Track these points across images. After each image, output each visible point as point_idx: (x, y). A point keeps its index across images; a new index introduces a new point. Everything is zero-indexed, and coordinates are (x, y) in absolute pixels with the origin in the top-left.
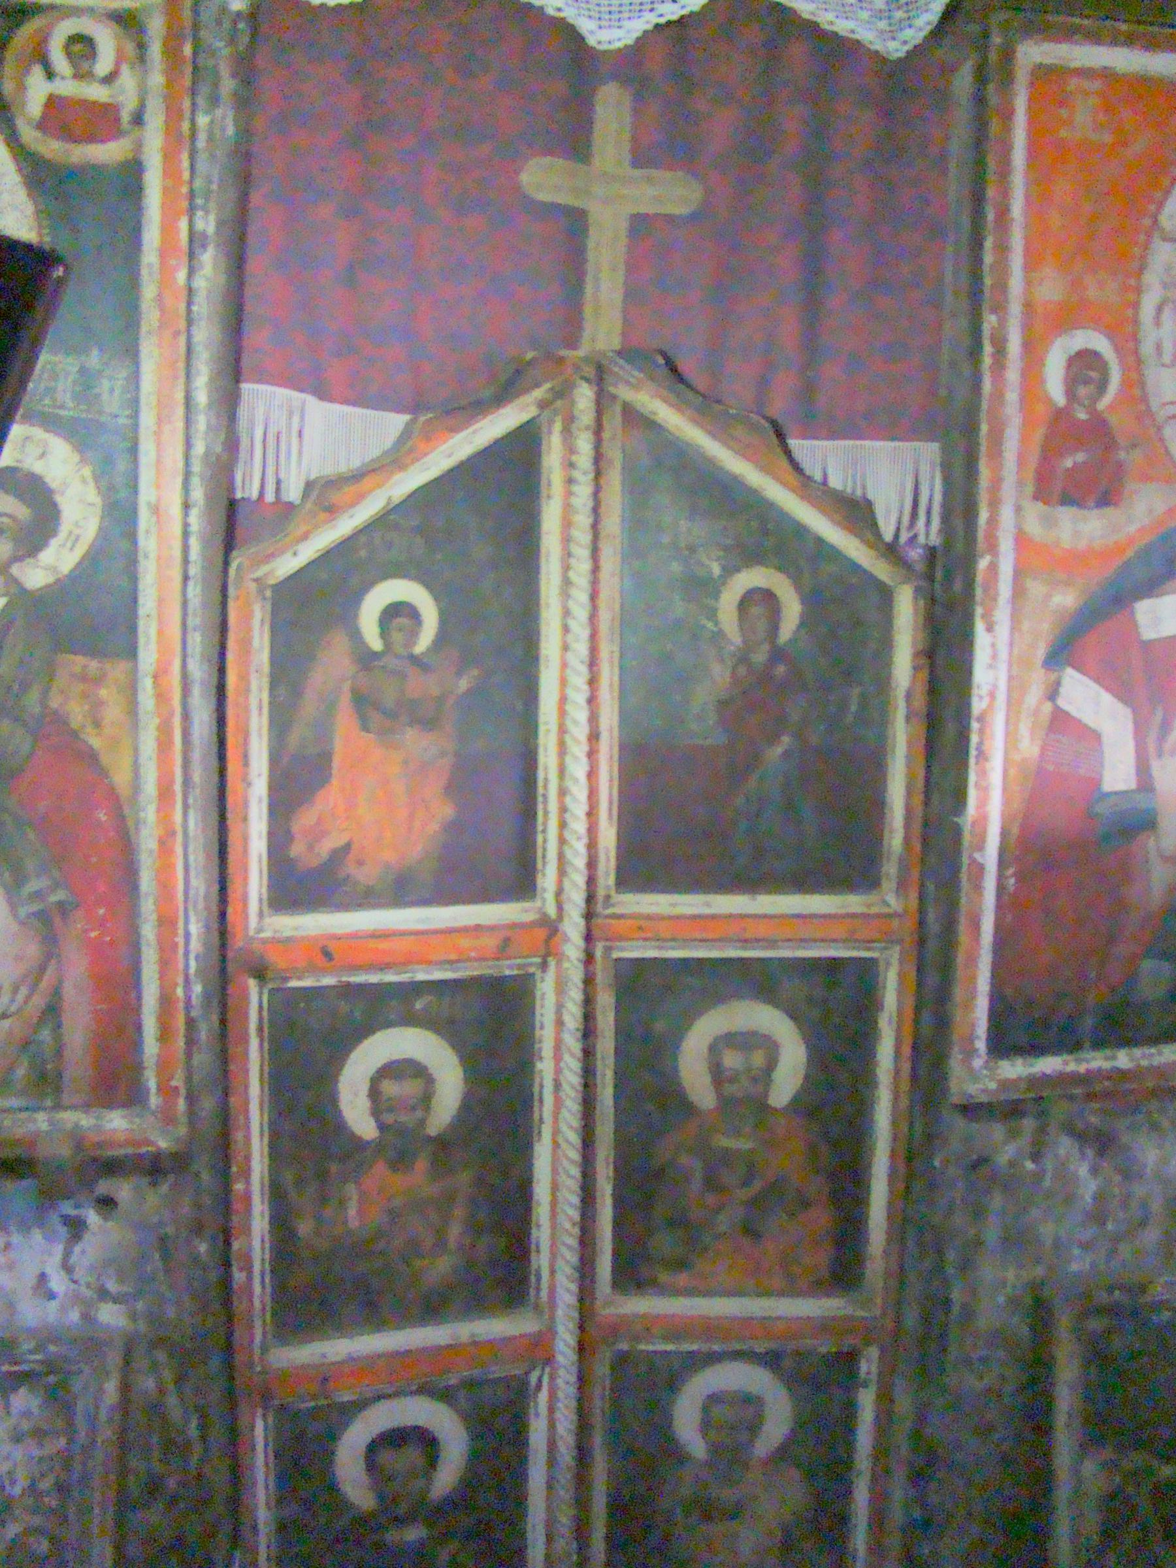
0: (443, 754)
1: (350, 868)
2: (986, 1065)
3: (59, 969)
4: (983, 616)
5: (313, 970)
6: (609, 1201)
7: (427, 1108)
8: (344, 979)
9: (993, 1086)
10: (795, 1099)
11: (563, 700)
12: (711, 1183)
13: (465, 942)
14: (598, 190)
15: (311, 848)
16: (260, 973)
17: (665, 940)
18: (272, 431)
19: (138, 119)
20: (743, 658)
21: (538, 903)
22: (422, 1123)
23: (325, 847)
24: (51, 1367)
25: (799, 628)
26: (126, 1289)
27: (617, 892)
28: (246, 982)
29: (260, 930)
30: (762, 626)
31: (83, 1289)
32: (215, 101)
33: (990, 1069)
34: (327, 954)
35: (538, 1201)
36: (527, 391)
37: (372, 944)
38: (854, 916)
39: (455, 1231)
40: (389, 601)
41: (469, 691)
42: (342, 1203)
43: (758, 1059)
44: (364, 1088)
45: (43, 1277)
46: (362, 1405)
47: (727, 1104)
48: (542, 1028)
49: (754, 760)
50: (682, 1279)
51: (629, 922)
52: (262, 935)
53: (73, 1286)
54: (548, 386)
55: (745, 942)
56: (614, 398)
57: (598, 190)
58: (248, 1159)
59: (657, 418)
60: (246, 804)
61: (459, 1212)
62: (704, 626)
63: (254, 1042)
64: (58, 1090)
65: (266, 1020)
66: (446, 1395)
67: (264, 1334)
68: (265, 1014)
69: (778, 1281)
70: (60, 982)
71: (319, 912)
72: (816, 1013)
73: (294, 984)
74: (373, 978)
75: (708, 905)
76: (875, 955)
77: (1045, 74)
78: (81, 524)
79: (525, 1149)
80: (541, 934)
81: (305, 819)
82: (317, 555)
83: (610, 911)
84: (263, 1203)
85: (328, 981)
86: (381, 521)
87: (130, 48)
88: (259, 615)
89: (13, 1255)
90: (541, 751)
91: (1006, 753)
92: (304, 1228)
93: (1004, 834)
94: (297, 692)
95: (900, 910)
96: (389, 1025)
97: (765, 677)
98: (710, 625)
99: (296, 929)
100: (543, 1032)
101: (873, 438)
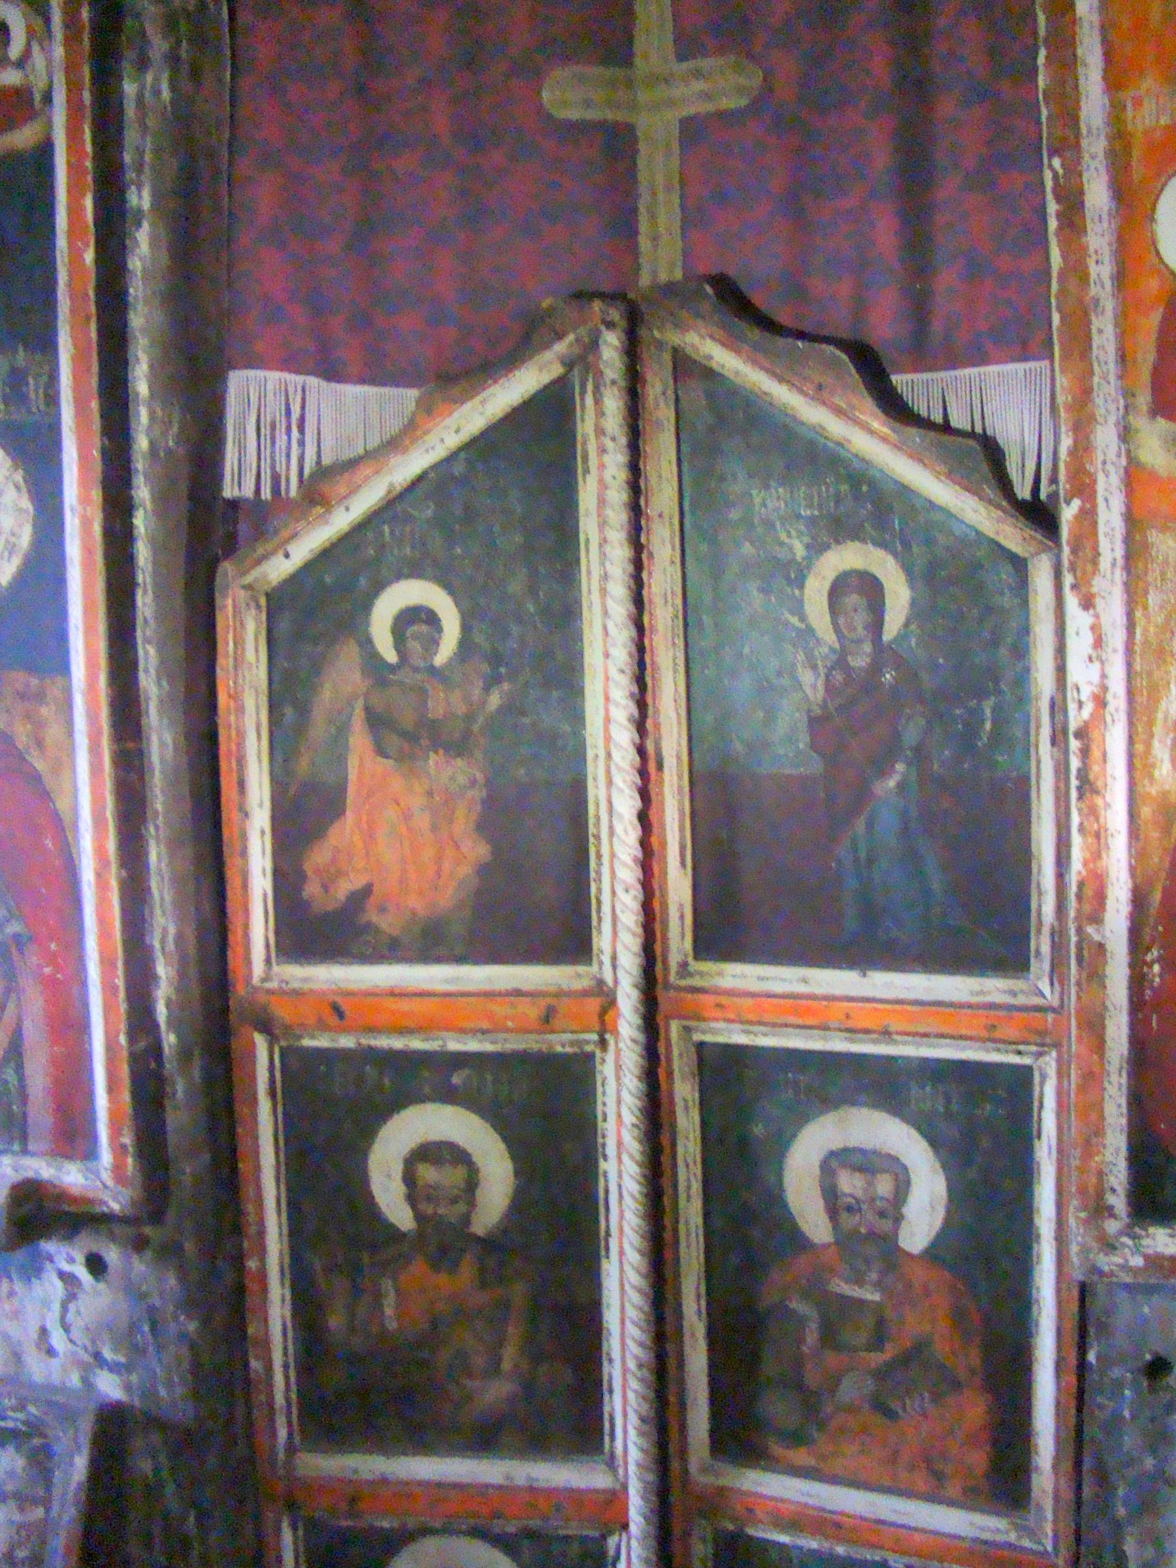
0: (473, 782)
2: (1128, 1231)
3: (19, 1006)
4: (1074, 587)
6: (702, 1345)
7: (472, 1204)
8: (364, 1041)
9: (1137, 1261)
11: (607, 720)
12: (830, 1336)
14: (643, 96)
15: (326, 888)
16: (266, 1026)
17: (751, 1023)
18: (266, 420)
19: (48, 98)
20: (841, 662)
21: (595, 968)
22: (466, 1220)
23: (344, 889)
24: (35, 1428)
25: (906, 625)
26: (122, 1359)
27: (696, 958)
28: (252, 1036)
30: (860, 620)
31: (82, 1352)
32: (143, 63)
33: (1135, 1237)
34: (338, 1011)
36: (547, 346)
37: (391, 1004)
38: (991, 1006)
39: (510, 1355)
40: (437, 610)
41: (500, 710)
42: (378, 1297)
43: (884, 1186)
44: (398, 1169)
45: (44, 1331)
47: (845, 1241)
48: (605, 1120)
49: (862, 795)
50: (801, 1456)
52: (268, 985)
53: (70, 1346)
55: (852, 1032)
56: (660, 345)
57: (643, 96)
58: (262, 1233)
60: (244, 838)
61: (514, 1332)
63: (264, 1107)
64: (24, 1138)
65: (279, 1084)
67: (290, 1434)
68: (278, 1075)
70: (52, 81)
71: (337, 962)
72: (953, 1133)
73: (307, 1042)
74: (398, 1043)
75: (805, 981)
76: (1026, 1061)
78: (16, 530)
81: (318, 857)
83: (683, 983)
84: (283, 1284)
85: (347, 1042)
87: (38, 23)
88: (253, 627)
89: (16, 1301)
90: (590, 783)
91: (1132, 784)
92: (335, 1321)
93: (1139, 900)
94: (304, 711)
95: (1056, 1003)
96: (422, 1099)
97: (869, 683)
98: (794, 620)
100: (606, 1125)
101: (998, 362)
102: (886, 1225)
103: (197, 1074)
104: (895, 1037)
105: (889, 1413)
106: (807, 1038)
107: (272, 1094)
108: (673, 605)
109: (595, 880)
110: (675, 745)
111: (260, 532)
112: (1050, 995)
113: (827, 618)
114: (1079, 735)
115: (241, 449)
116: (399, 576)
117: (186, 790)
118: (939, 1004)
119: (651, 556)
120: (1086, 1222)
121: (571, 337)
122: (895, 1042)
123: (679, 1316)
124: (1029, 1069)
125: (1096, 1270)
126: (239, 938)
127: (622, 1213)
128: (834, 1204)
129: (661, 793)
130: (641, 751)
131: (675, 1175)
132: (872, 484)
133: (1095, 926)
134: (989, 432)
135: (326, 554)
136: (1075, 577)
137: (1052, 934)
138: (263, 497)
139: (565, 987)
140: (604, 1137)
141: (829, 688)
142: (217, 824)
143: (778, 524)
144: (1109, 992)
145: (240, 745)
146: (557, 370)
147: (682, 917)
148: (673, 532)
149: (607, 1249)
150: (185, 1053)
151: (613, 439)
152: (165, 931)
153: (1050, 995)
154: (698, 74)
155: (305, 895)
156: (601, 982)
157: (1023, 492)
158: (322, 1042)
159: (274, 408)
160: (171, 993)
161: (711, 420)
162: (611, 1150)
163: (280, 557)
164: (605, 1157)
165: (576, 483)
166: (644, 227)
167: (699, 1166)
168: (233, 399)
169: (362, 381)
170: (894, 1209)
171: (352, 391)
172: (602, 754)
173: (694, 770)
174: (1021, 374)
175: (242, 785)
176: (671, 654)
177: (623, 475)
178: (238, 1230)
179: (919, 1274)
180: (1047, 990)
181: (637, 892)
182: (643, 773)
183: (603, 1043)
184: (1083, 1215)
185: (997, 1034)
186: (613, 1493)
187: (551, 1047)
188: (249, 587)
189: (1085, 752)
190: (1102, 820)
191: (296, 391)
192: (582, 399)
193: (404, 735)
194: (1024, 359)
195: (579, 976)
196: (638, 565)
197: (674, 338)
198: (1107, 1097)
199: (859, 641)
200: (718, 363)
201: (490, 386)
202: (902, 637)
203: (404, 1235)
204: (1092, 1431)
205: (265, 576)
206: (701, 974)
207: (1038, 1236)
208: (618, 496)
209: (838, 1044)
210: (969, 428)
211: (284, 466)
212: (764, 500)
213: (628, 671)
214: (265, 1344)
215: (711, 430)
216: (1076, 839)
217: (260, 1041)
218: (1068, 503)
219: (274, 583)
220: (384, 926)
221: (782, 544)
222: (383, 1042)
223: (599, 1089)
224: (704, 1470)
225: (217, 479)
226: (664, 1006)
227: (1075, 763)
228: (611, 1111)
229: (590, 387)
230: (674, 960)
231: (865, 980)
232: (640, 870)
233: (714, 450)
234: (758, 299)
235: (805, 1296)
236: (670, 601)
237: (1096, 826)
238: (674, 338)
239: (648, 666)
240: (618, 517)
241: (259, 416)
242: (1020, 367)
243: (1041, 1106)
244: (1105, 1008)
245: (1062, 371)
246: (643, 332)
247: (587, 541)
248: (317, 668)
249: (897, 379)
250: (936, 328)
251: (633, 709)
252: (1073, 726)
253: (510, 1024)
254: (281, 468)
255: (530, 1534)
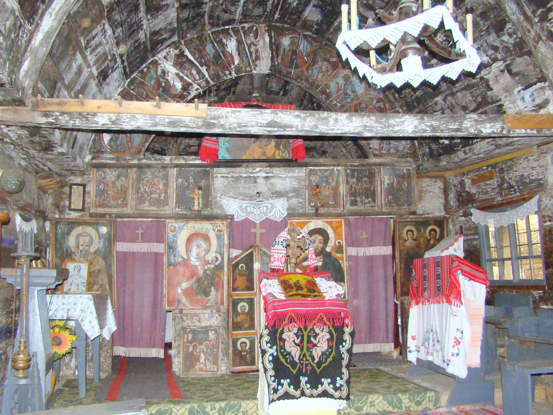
46: (240, 338)
66: (247, 338)
77: (290, 222)
79: (254, 314)
81: (235, 284)
86: (241, 259)
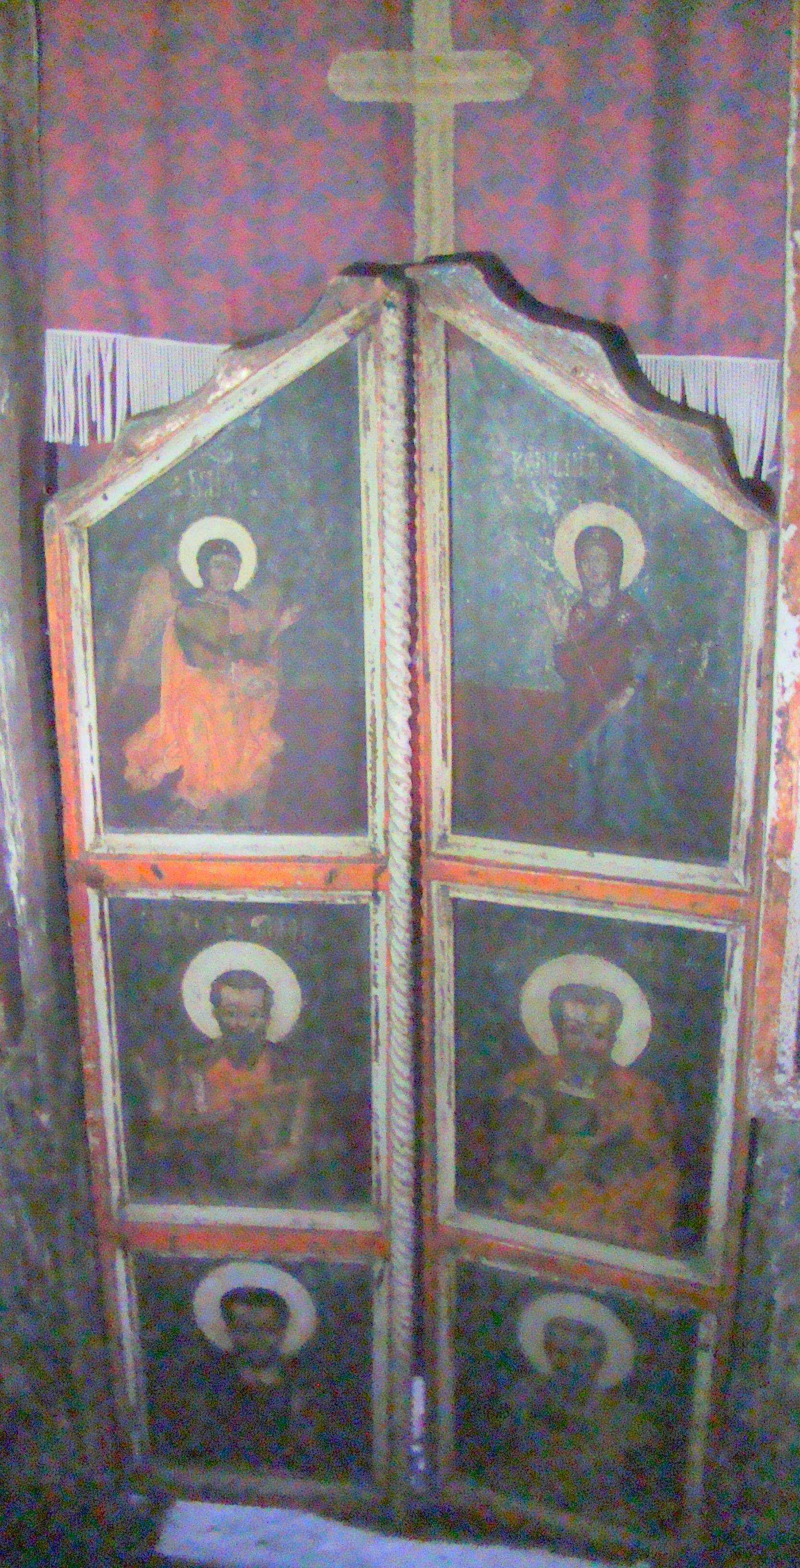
1: (182, 793)
5: (145, 884)
8: (178, 894)
10: (639, 1060)
11: (383, 643)
12: (553, 1125)
13: (292, 871)
15: (144, 771)
16: (96, 882)
20: (584, 604)
21: (370, 838)
22: (262, 1032)
23: (158, 773)
25: (641, 576)
27: (453, 832)
29: (97, 845)
30: (602, 567)
34: (157, 872)
35: (376, 1114)
38: (694, 888)
41: (292, 629)
42: (191, 1090)
43: (601, 1015)
44: (206, 991)
47: (567, 1053)
48: (376, 956)
49: (597, 708)
50: (526, 1209)
51: (462, 865)
52: (98, 851)
54: (355, 311)
56: (433, 318)
58: (97, 1043)
59: (481, 340)
60: (74, 730)
62: (539, 566)
69: (620, 1231)
73: (131, 895)
74: (206, 896)
75: (544, 856)
76: (721, 930)
80: (368, 869)
82: (126, 499)
83: (441, 852)
84: (114, 1080)
85: (164, 895)
92: (157, 1106)
94: (122, 625)
95: (747, 889)
96: (226, 938)
97: (606, 621)
99: (129, 847)
101: (734, 354)
102: (602, 1044)
103: (43, 927)
104: (615, 905)
105: (600, 1183)
106: (544, 901)
107: (103, 935)
108: (441, 545)
109: (371, 769)
110: (440, 662)
111: (79, 477)
112: (742, 881)
113: (573, 563)
114: (780, 713)
115: (61, 397)
116: (201, 515)
117: (27, 701)
118: (651, 883)
119: (423, 504)
120: (761, 1075)
121: (355, 311)
122: (616, 910)
123: (433, 1103)
124: (722, 938)
125: (766, 1110)
126: (73, 812)
127: (390, 1030)
128: (558, 1021)
129: (428, 701)
130: (412, 668)
131: (433, 1000)
132: (617, 455)
133: (784, 859)
134: (722, 415)
135: (142, 495)
136: (787, 588)
137: (748, 835)
138: (81, 444)
139: (345, 854)
140: (375, 969)
141: (573, 625)
142: (52, 724)
143: (534, 483)
144: (791, 909)
145: (70, 658)
146: (343, 339)
147: (443, 800)
148: (442, 482)
149: (377, 1054)
150: (32, 912)
151: (393, 407)
152: (14, 817)
153: (742, 881)
154: (472, 65)
155: (126, 777)
156: (374, 850)
157: (747, 471)
158: (143, 894)
159: (89, 365)
160: (21, 865)
161: (476, 385)
162: (381, 980)
163: (99, 499)
164: (376, 985)
165: (358, 435)
166: (418, 201)
167: (452, 993)
168: (51, 355)
169: (166, 335)
170: (609, 1034)
171: (157, 343)
172: (378, 666)
173: (456, 681)
174: (752, 368)
175: (71, 690)
176: (439, 584)
177: (401, 438)
178: (77, 1037)
179: (625, 1084)
180: (741, 879)
181: (407, 784)
182: (413, 685)
183: (376, 898)
184: (758, 1070)
185: (698, 909)
186: (379, 1234)
187: (332, 900)
188: (73, 524)
189: (784, 727)
190: (794, 780)
191: (107, 348)
192: (364, 367)
193: (208, 645)
194: (756, 355)
195: (356, 844)
196: (412, 513)
197: (446, 313)
198: (783, 986)
199: (600, 586)
200: (486, 340)
201: (283, 354)
202: (634, 585)
203: (212, 1041)
204: (757, 1214)
205: (86, 514)
206: (458, 845)
207: (722, 1061)
208: (396, 457)
209: (569, 907)
210: (704, 410)
211: (99, 417)
212: (522, 460)
213: (402, 605)
214: (100, 1124)
215: (479, 394)
216: (773, 793)
217: (92, 895)
218: (786, 527)
219: (95, 521)
220: (193, 802)
221: (536, 500)
222: (193, 895)
223: (372, 933)
224: (451, 1217)
225: (41, 428)
226: (426, 871)
227: (776, 735)
228: (382, 948)
229: (371, 353)
230: (436, 832)
231: (593, 859)
232: (410, 767)
233: (482, 415)
234: (523, 279)
235: (535, 1093)
236: (438, 541)
237: (789, 785)
238: (446, 313)
239: (419, 598)
240: (396, 476)
241: (75, 369)
242: (752, 362)
243: (731, 966)
244: (786, 922)
245: (789, 417)
246: (420, 309)
247: (368, 488)
248: (133, 588)
249: (644, 359)
250: (680, 311)
251: (406, 636)
252: (776, 706)
253: (299, 883)
254: (96, 415)
255: (315, 1264)
